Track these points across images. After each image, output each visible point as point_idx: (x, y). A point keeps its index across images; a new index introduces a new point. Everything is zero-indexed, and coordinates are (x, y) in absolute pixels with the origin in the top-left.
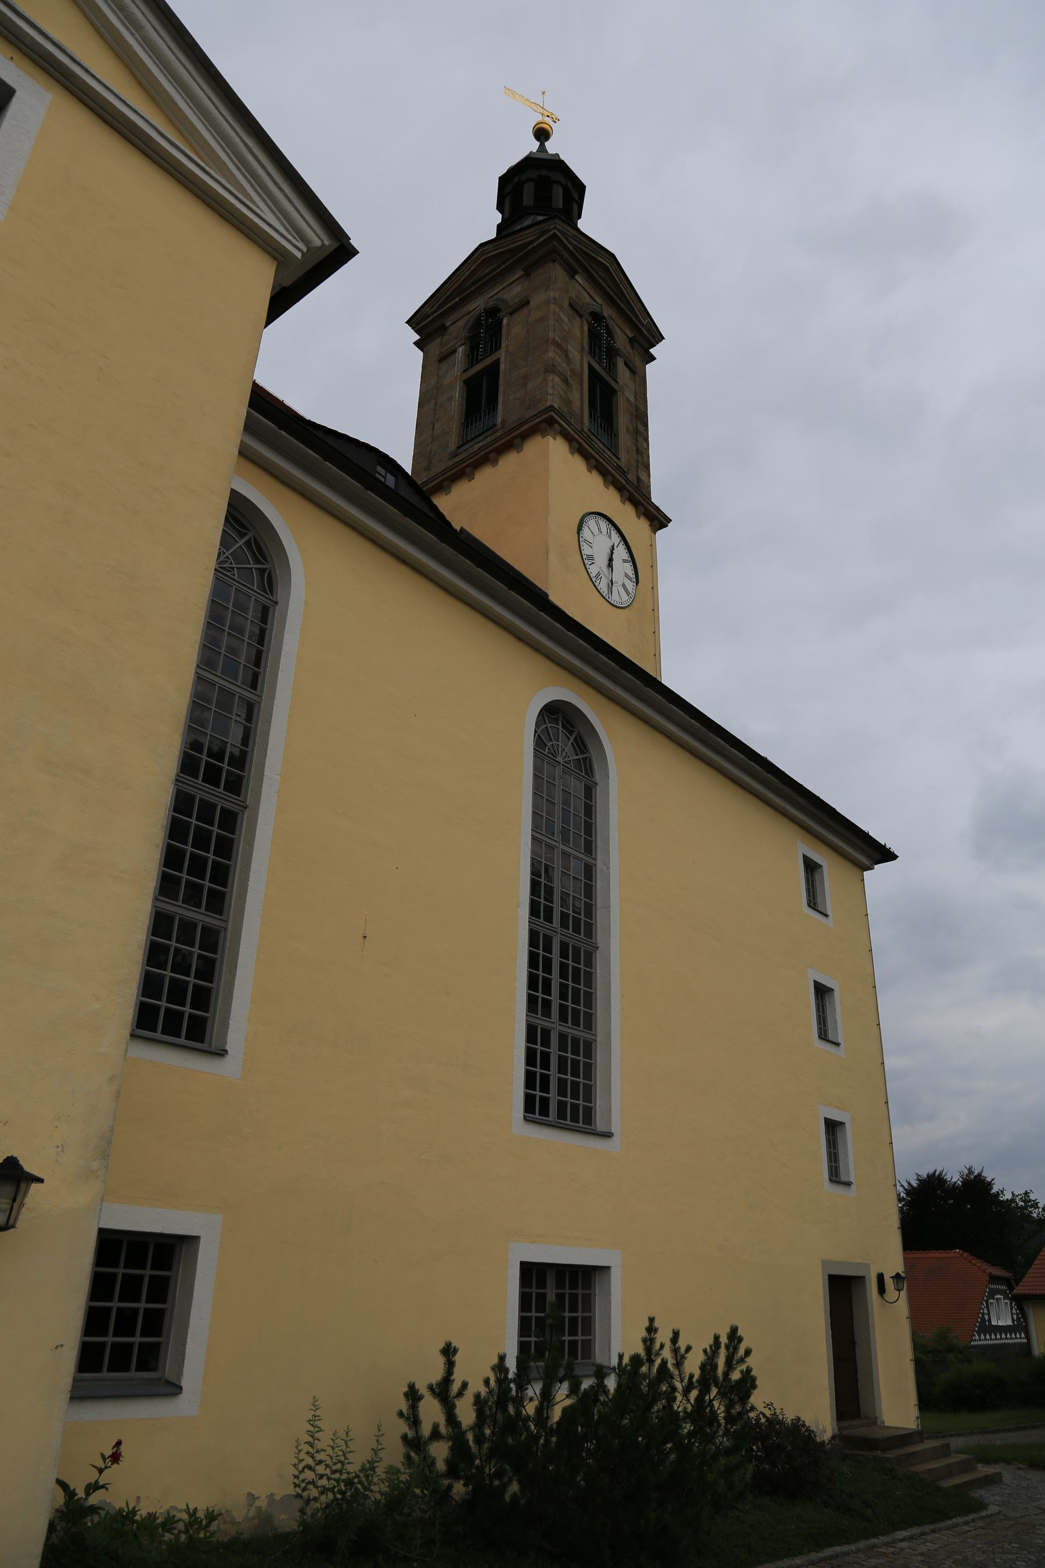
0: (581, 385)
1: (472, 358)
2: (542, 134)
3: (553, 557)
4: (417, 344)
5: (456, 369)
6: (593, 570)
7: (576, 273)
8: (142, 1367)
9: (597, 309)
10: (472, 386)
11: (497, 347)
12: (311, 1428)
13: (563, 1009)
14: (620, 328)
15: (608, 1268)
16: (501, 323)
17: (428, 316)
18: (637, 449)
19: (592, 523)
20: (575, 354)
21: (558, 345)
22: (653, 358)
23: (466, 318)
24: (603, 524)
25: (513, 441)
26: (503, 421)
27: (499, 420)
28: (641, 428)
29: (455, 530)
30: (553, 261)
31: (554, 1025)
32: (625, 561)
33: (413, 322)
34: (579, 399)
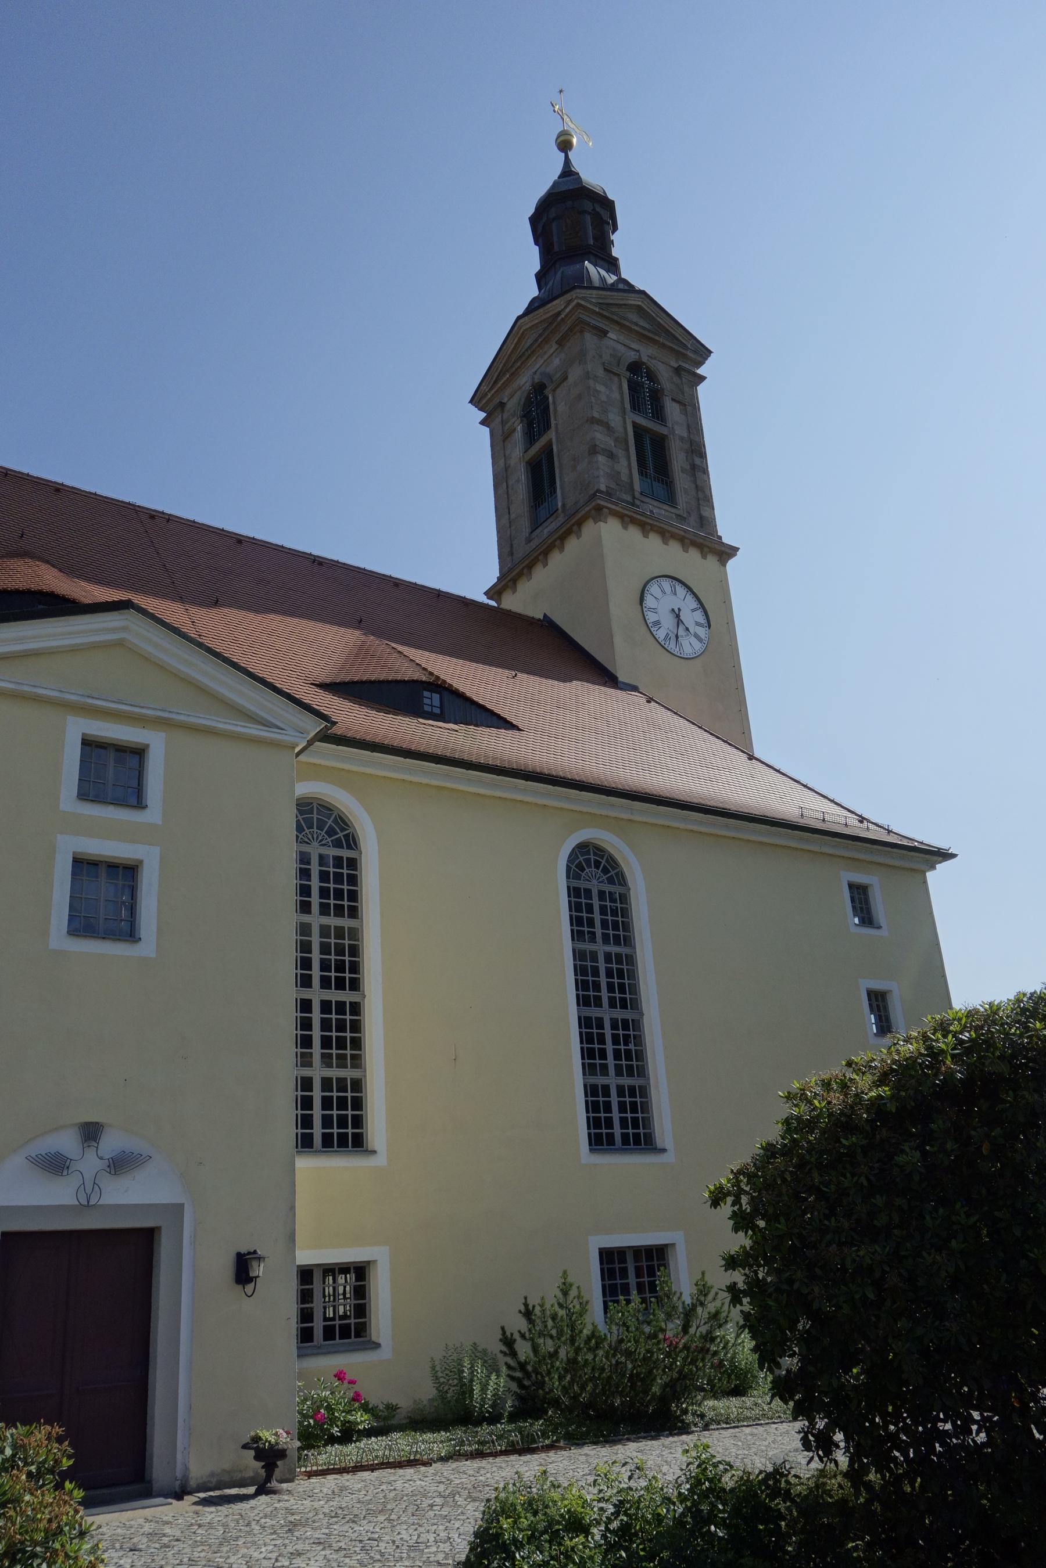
0: (627, 450)
1: (531, 437)
3: (618, 640)
4: (482, 423)
5: (517, 451)
6: (661, 635)
7: (607, 332)
8: (357, 1335)
9: (632, 356)
11: (549, 427)
17: (486, 394)
18: (697, 486)
19: (654, 589)
20: (614, 418)
21: (599, 422)
22: (702, 378)
23: (518, 393)
24: (666, 584)
25: (572, 528)
26: (564, 505)
27: (560, 504)
28: (698, 461)
29: (539, 620)
30: (581, 332)
32: (693, 610)
34: (627, 465)
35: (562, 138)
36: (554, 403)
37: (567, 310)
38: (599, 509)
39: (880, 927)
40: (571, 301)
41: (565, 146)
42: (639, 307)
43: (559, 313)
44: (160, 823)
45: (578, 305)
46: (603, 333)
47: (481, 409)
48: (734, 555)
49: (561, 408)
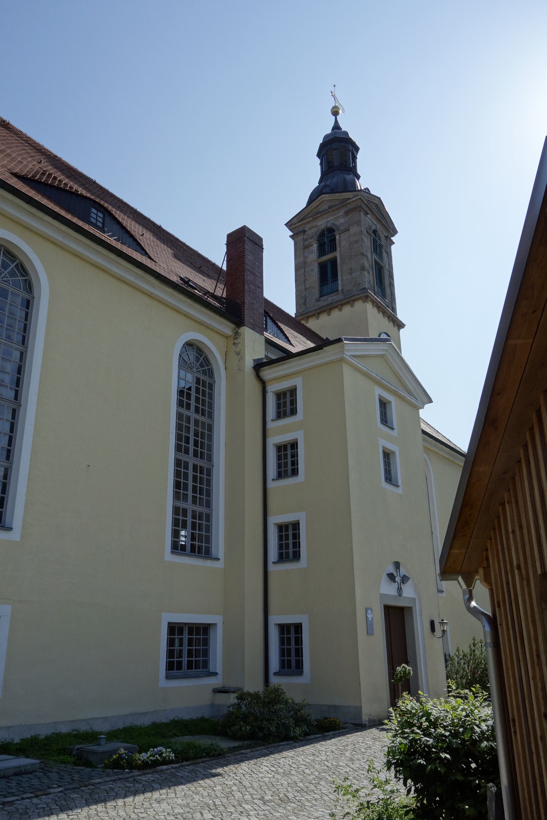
1: (322, 252)
2: (335, 113)
4: (291, 237)
7: (368, 214)
10: (323, 267)
11: (333, 249)
12: (71, 777)
13: (194, 498)
14: (380, 229)
15: (216, 624)
16: (335, 238)
17: (296, 224)
20: (369, 255)
30: (360, 211)
31: (191, 460)
33: (290, 225)
35: (335, 109)
36: (339, 240)
37: (354, 199)
38: (367, 297)
39: (398, 486)
40: (357, 195)
41: (335, 113)
42: (377, 204)
43: (349, 199)
44: (303, 431)
45: (361, 198)
46: (366, 214)
47: (290, 230)
48: (403, 328)
49: (344, 243)
